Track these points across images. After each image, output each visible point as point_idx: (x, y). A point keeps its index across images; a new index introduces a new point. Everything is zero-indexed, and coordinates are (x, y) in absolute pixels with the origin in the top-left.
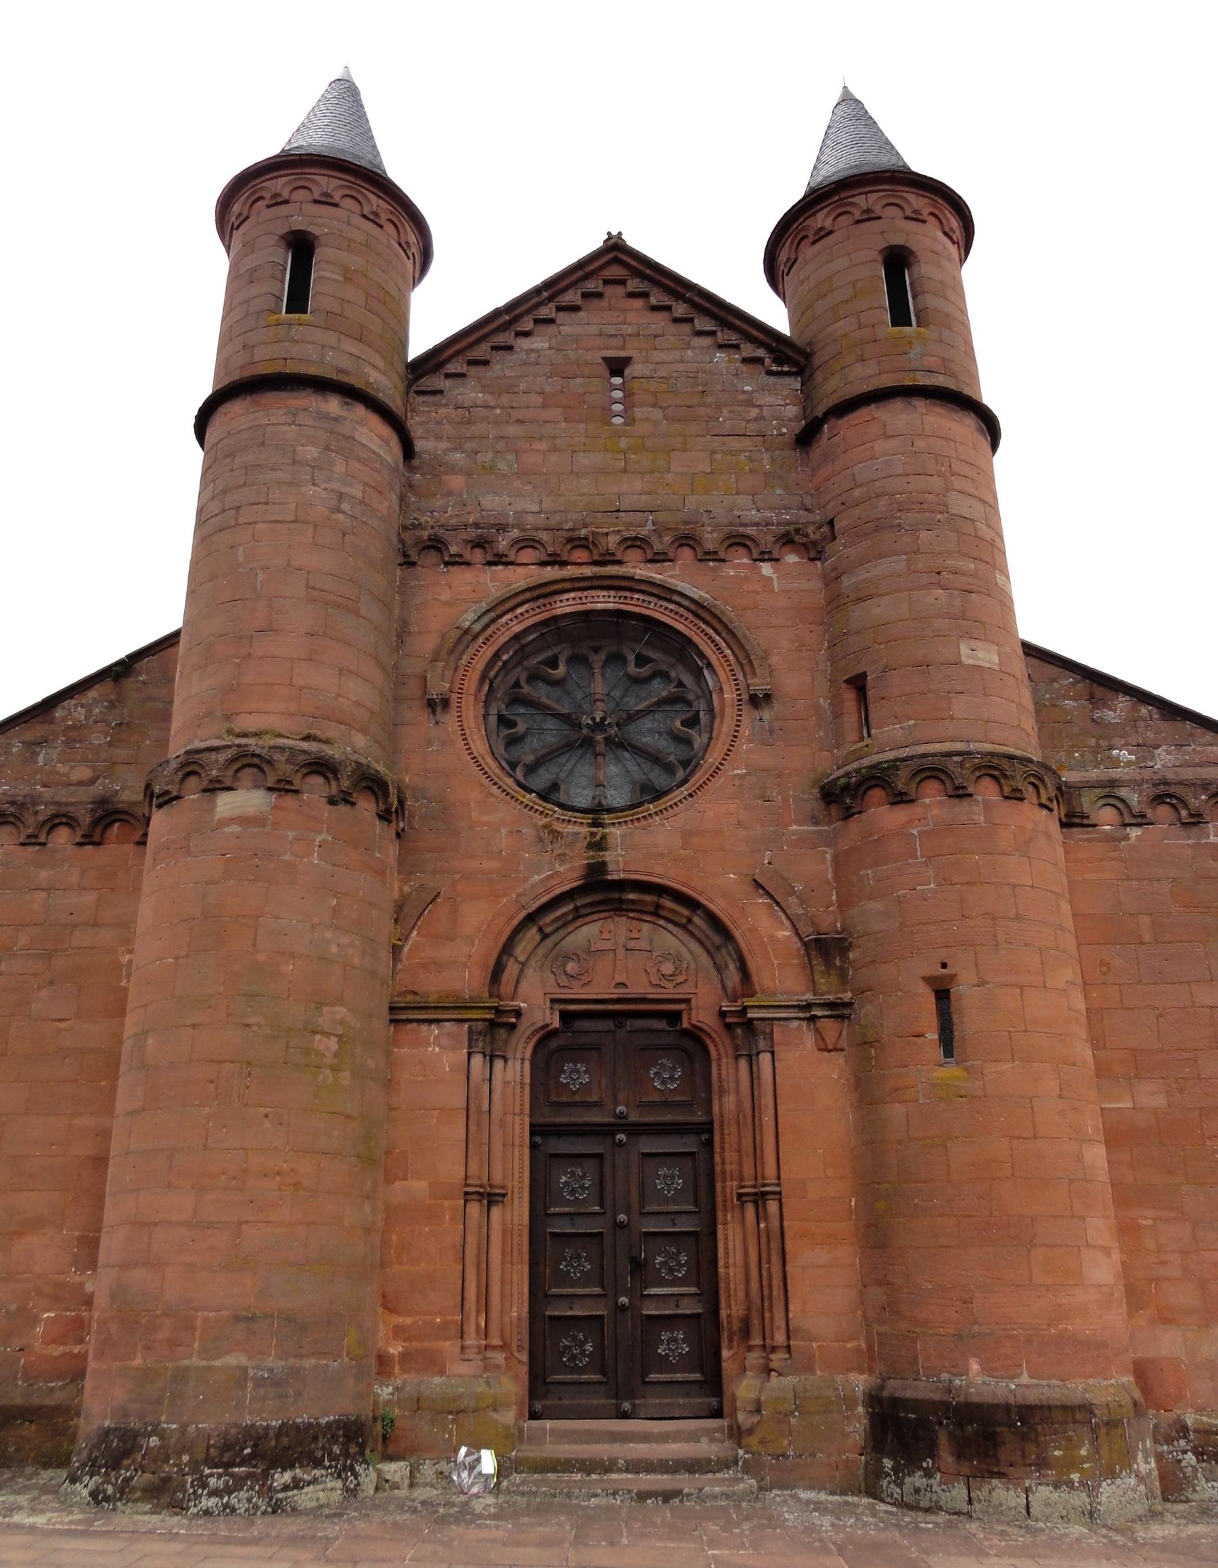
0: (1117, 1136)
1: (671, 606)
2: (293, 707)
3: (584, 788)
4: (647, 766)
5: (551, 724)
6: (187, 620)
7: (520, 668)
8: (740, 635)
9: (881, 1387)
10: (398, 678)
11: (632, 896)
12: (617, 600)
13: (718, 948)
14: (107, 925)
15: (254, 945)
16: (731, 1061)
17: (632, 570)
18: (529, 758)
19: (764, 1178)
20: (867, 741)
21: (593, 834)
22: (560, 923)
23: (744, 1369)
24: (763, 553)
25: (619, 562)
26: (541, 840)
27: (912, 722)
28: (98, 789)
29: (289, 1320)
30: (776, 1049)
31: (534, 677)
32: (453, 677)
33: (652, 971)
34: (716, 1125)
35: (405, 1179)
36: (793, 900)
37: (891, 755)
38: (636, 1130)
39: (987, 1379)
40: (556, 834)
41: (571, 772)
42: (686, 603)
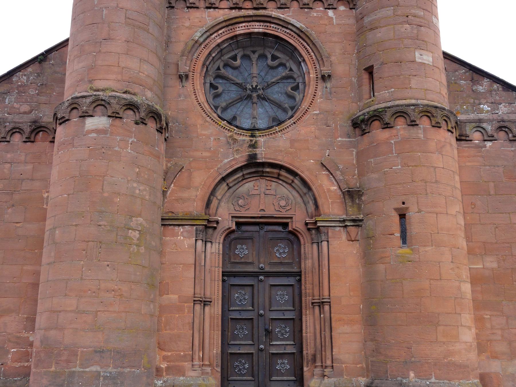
0: (476, 280)
1: (288, 31)
2: (119, 77)
3: (247, 119)
4: (275, 109)
5: (234, 88)
6: (72, 34)
7: (220, 60)
8: (318, 46)
9: (372, 383)
10: (166, 64)
11: (268, 170)
12: (264, 27)
13: (305, 194)
14: (37, 180)
15: (102, 189)
16: (310, 245)
17: (270, 13)
18: (224, 104)
19: (323, 296)
20: (373, 98)
21: (251, 141)
22: (236, 182)
23: (313, 375)
24: (329, 5)
25: (265, 8)
26: (228, 143)
27: (393, 90)
28: (32, 116)
29: (118, 352)
30: (329, 240)
31: (226, 65)
32: (190, 64)
33: (276, 204)
34: (303, 273)
35: (168, 294)
36: (338, 173)
37: (383, 105)
38: (268, 275)
39: (417, 380)
40: (235, 140)
41: (242, 111)
42: (294, 29)
